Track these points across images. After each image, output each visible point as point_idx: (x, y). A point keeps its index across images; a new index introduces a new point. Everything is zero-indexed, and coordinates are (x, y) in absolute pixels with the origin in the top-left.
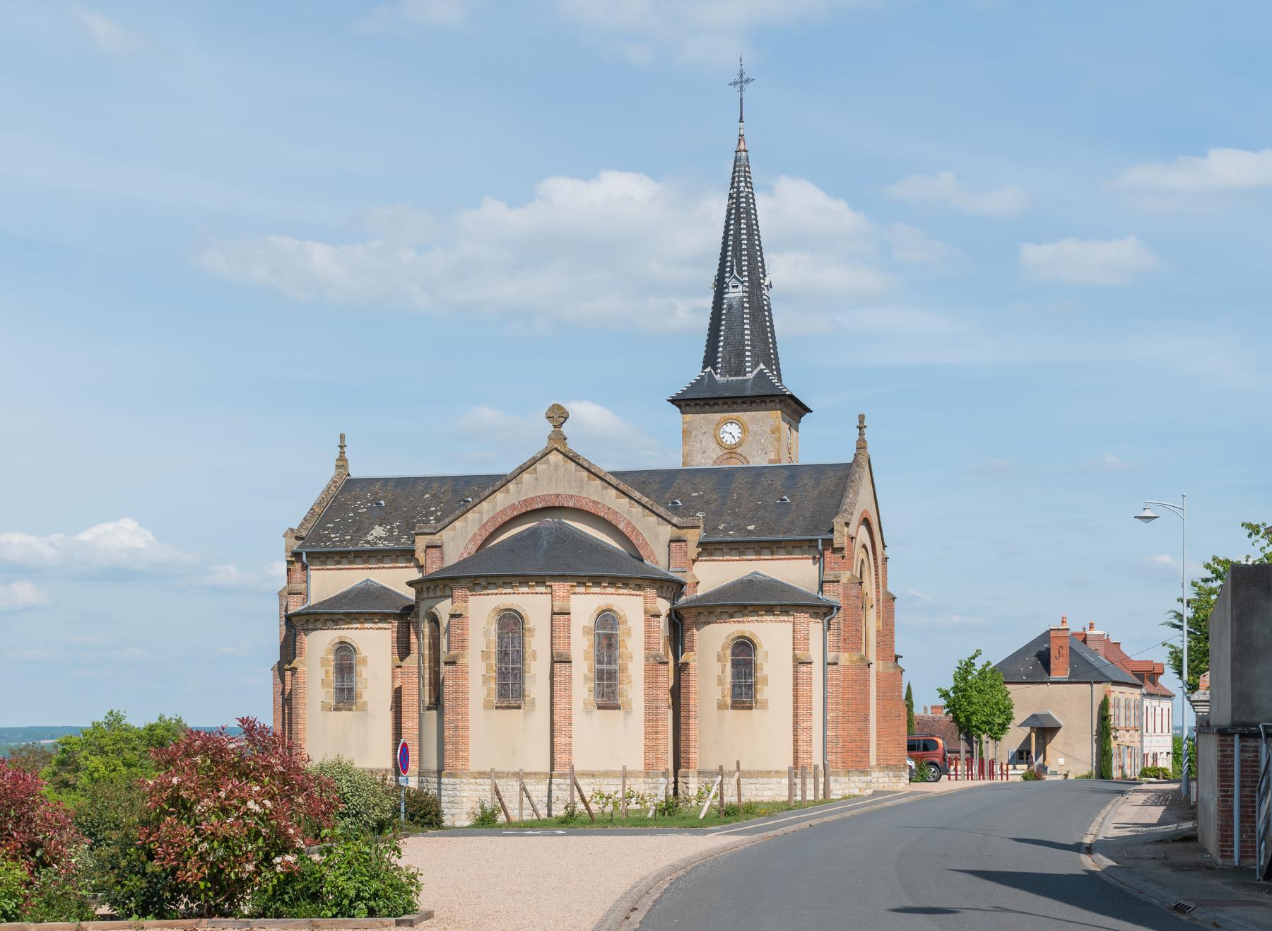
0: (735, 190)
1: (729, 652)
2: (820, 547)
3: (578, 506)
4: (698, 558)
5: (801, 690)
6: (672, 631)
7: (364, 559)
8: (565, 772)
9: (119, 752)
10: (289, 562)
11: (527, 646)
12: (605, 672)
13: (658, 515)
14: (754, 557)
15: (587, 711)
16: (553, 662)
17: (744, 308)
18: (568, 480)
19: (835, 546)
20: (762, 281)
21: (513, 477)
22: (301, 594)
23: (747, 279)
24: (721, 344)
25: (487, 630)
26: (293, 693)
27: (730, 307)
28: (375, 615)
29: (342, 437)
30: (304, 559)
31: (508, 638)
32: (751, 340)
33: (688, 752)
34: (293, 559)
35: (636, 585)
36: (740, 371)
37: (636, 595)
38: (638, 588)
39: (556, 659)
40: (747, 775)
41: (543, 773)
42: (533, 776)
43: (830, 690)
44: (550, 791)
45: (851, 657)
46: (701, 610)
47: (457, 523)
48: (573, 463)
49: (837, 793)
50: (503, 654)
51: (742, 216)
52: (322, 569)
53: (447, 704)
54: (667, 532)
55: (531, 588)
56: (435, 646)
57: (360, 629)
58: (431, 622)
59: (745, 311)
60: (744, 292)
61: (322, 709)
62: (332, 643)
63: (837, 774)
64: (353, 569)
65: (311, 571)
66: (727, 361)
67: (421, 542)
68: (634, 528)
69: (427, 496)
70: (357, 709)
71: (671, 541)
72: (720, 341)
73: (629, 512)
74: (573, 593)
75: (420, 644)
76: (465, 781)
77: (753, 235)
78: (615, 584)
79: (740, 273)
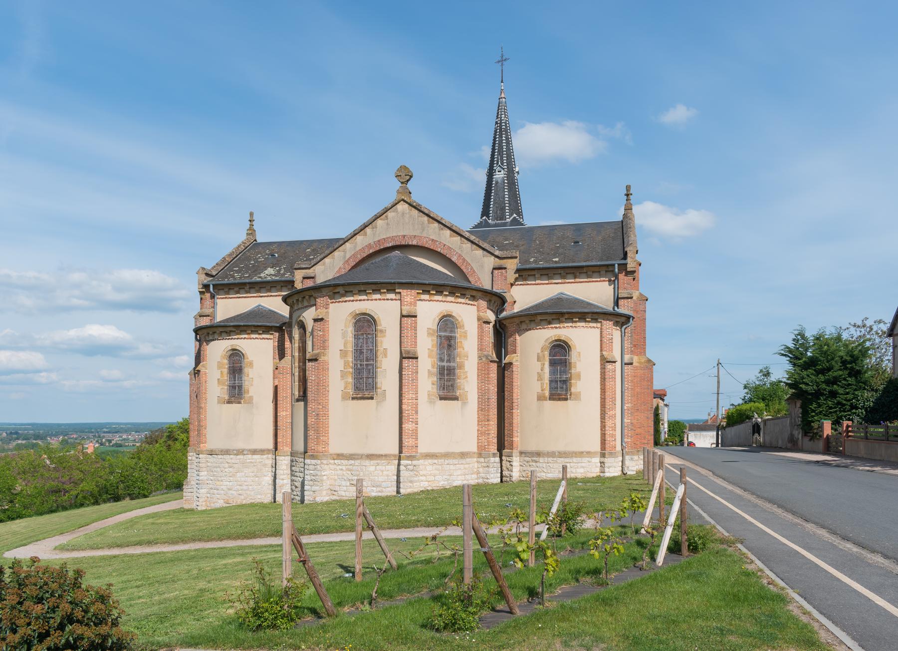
0: (499, 119)
1: (547, 353)
2: (617, 270)
3: (420, 244)
4: (515, 283)
5: (607, 384)
6: (496, 339)
7: (257, 289)
8: (412, 454)
10: (201, 293)
11: (379, 345)
12: (445, 368)
13: (484, 249)
14: (560, 281)
15: (431, 402)
16: (402, 358)
17: (504, 183)
18: (412, 224)
19: (628, 270)
20: (514, 169)
21: (370, 223)
22: (208, 316)
23: (506, 167)
24: (492, 203)
27: (497, 183)
28: (259, 328)
29: (251, 214)
30: (211, 289)
31: (363, 339)
32: (508, 201)
33: (511, 436)
34: (204, 290)
35: (471, 296)
36: (503, 217)
37: (471, 305)
38: (472, 298)
39: (404, 356)
42: (384, 458)
43: (627, 386)
44: (399, 471)
45: (640, 359)
46: (523, 319)
47: (327, 260)
48: (416, 211)
49: (633, 469)
50: (358, 352)
51: (503, 133)
52: (226, 298)
53: (310, 395)
54: (491, 261)
55: (383, 295)
56: (303, 349)
57: (248, 339)
58: (300, 328)
59: (506, 184)
60: (504, 174)
62: (226, 350)
63: (632, 454)
64: (248, 297)
66: (495, 212)
68: (464, 260)
69: (308, 250)
70: (245, 403)
71: (494, 269)
72: (491, 202)
73: (460, 248)
74: (419, 300)
75: (292, 347)
76: (325, 462)
77: (509, 144)
78: (454, 293)
79: (502, 164)
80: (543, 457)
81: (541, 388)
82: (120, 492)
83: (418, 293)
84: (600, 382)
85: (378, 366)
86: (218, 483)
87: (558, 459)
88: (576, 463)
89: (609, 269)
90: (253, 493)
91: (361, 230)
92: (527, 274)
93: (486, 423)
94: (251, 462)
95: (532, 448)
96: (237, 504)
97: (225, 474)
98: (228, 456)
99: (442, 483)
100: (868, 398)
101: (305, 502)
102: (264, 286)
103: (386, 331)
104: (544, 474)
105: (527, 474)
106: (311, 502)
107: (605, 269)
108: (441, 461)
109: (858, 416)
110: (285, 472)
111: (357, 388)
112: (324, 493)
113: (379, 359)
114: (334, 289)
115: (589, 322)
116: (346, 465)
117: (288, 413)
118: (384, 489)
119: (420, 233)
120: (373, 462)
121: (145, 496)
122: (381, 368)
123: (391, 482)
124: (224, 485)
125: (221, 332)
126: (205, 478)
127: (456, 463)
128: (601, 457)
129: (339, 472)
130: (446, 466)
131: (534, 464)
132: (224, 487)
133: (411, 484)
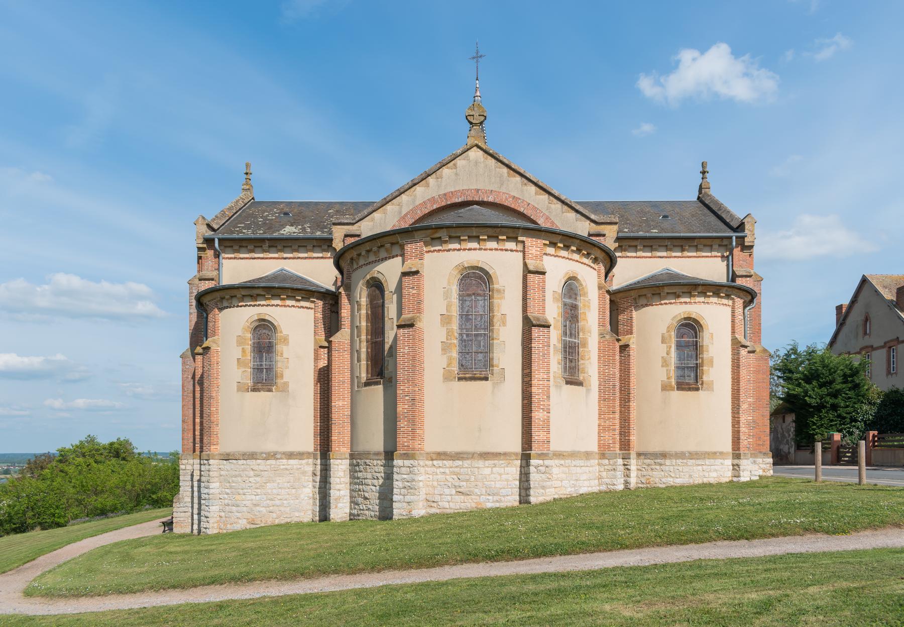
3: (497, 201)
8: (545, 452)
9: (93, 456)
10: (200, 249)
11: (496, 309)
13: (577, 211)
19: (746, 244)
22: (212, 279)
25: (448, 290)
26: (205, 375)
28: (298, 292)
30: (217, 245)
34: (205, 246)
40: (695, 457)
41: (514, 454)
42: (502, 457)
48: (493, 160)
52: (235, 258)
55: (501, 243)
57: (282, 306)
62: (250, 321)
65: (223, 260)
70: (277, 390)
76: (421, 463)
80: (670, 459)
81: (667, 375)
82: (29, 521)
83: (545, 244)
84: (730, 370)
85: (495, 336)
86: (238, 497)
87: (688, 460)
88: (708, 465)
89: (722, 242)
90: (288, 509)
91: (423, 180)
92: (628, 244)
93: (611, 416)
94: (286, 469)
95: (655, 446)
96: (267, 525)
97: (250, 484)
98: (254, 461)
99: (569, 489)
100: (868, 411)
101: (394, 517)
102: (290, 245)
103: (504, 291)
104: (672, 479)
105: (648, 479)
106: (404, 517)
107: (718, 241)
108: (568, 462)
109: (858, 428)
110: (342, 480)
111: (462, 365)
112: (421, 504)
113: (496, 327)
115: (722, 297)
117: (346, 403)
118: (503, 498)
120: (488, 463)
121: (59, 525)
122: (499, 339)
123: (511, 488)
125: (244, 296)
126: (217, 491)
127: (582, 465)
128: (733, 458)
129: (439, 477)
130: (573, 468)
131: (658, 467)
132: (247, 502)
133: (542, 491)
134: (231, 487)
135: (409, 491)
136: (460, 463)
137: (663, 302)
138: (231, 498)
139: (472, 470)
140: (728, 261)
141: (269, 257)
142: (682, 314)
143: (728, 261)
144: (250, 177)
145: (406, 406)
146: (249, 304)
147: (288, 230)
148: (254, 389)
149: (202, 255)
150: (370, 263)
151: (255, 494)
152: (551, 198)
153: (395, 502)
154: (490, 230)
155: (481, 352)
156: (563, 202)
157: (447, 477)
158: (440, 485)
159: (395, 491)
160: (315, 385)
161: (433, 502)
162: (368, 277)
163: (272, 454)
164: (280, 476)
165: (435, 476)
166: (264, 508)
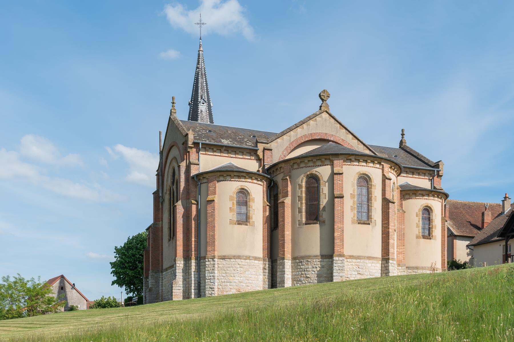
1: (421, 213)
3: (335, 140)
19: (440, 174)
42: (375, 259)
47: (278, 140)
48: (333, 120)
50: (385, 190)
61: (230, 224)
67: (261, 147)
81: (418, 232)
93: (403, 247)
97: (237, 272)
98: (240, 260)
107: (428, 172)
114: (348, 157)
116: (355, 262)
119: (335, 134)
123: (378, 273)
124: (237, 280)
125: (234, 176)
132: (236, 280)
134: (226, 273)
135: (341, 271)
136: (359, 260)
137: (417, 198)
138: (226, 279)
139: (364, 264)
140: (431, 181)
141: (223, 155)
142: (425, 204)
143: (431, 181)
144: (174, 105)
145: (339, 234)
146: (236, 180)
147: (225, 142)
148: (239, 223)
149: (190, 151)
150: (309, 166)
151: (240, 276)
152: (359, 142)
153: (335, 276)
154: (372, 158)
155: (365, 212)
156: (364, 145)
157: (353, 266)
158: (351, 270)
159: (334, 271)
160: (263, 225)
161: (347, 278)
162: (308, 173)
163: (248, 257)
164: (251, 268)
165: (348, 266)
166: (244, 284)
